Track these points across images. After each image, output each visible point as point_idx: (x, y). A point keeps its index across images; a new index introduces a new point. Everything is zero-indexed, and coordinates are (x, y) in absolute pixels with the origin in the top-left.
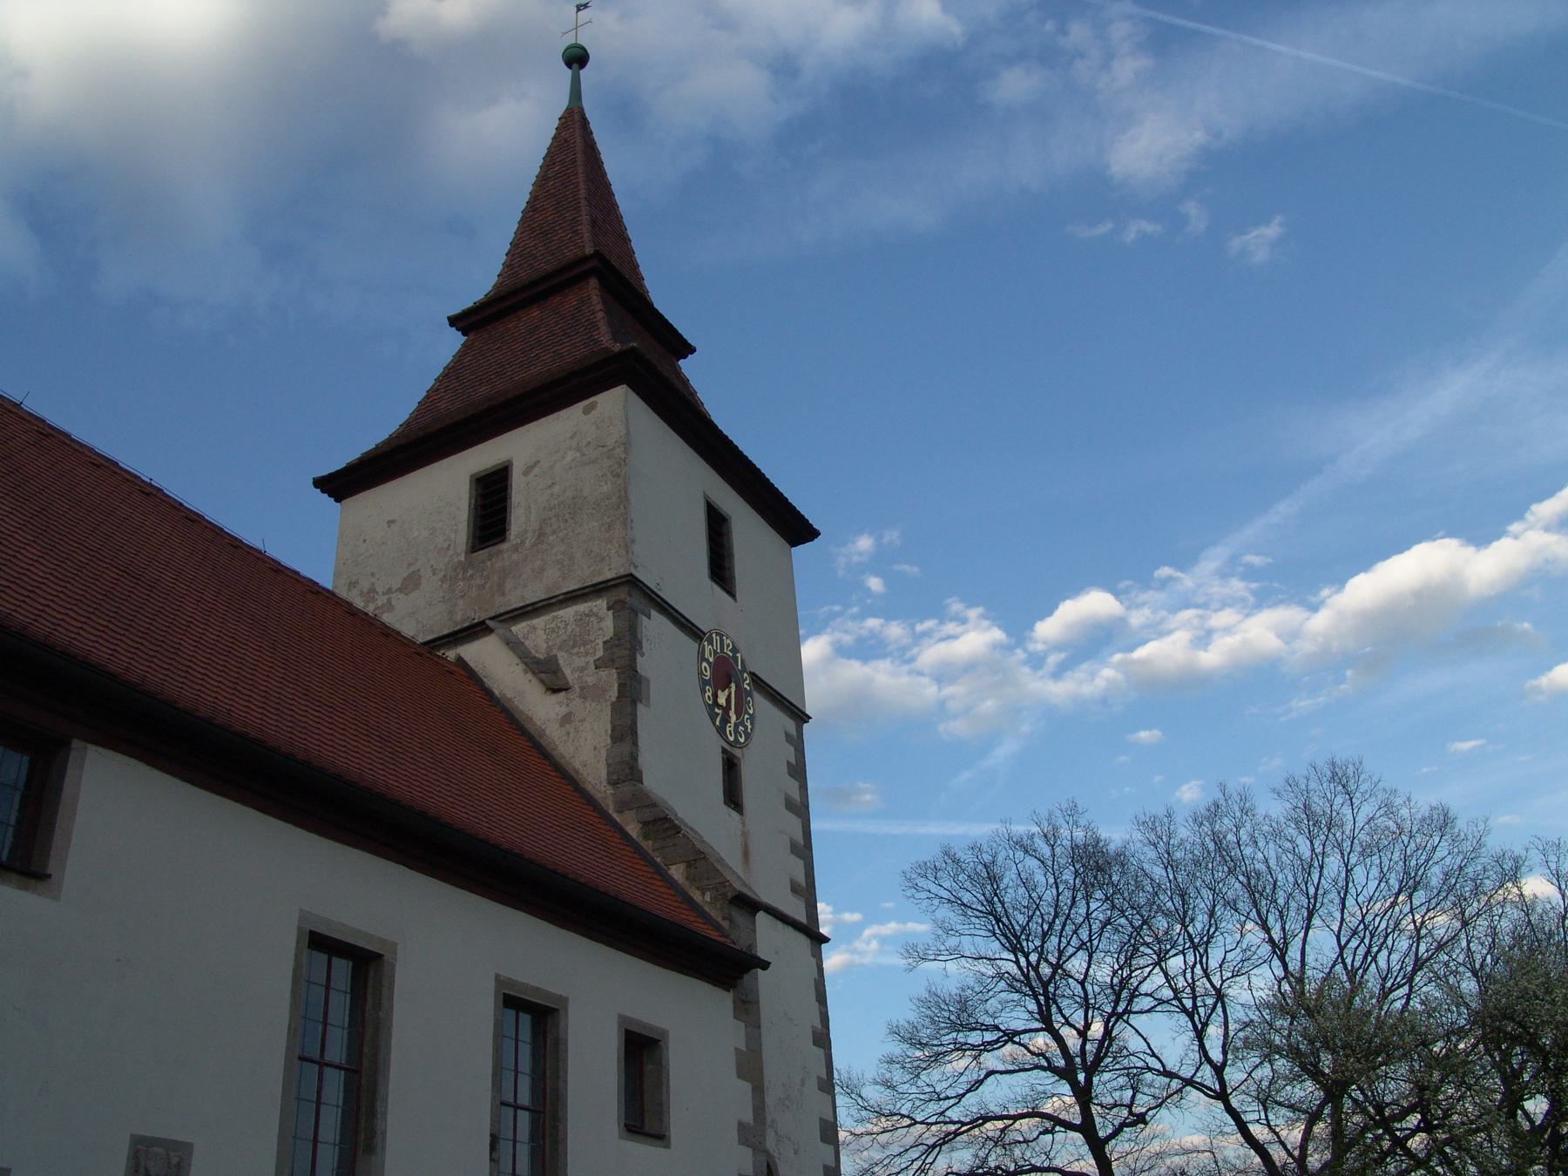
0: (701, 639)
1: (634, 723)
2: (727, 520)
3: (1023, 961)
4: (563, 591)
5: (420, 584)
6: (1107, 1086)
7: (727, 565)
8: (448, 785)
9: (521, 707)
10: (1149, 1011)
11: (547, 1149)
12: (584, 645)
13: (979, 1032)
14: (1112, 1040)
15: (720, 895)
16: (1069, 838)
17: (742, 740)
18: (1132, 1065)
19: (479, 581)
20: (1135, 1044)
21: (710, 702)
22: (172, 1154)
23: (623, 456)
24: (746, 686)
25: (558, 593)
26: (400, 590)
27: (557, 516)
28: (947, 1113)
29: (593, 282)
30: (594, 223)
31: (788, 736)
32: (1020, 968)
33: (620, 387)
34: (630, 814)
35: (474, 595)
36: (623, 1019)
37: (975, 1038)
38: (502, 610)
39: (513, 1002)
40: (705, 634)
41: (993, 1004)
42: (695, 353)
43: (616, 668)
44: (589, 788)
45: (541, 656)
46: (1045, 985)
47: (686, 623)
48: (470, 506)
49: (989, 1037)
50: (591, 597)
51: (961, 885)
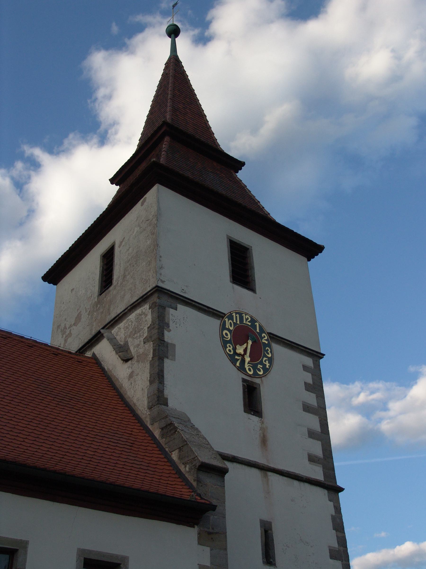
2: (248, 249)
12: (139, 332)
19: (101, 310)
23: (155, 222)
34: (156, 425)
36: (81, 552)
42: (245, 163)
44: (139, 413)
45: (122, 343)
47: (207, 309)
48: (100, 272)
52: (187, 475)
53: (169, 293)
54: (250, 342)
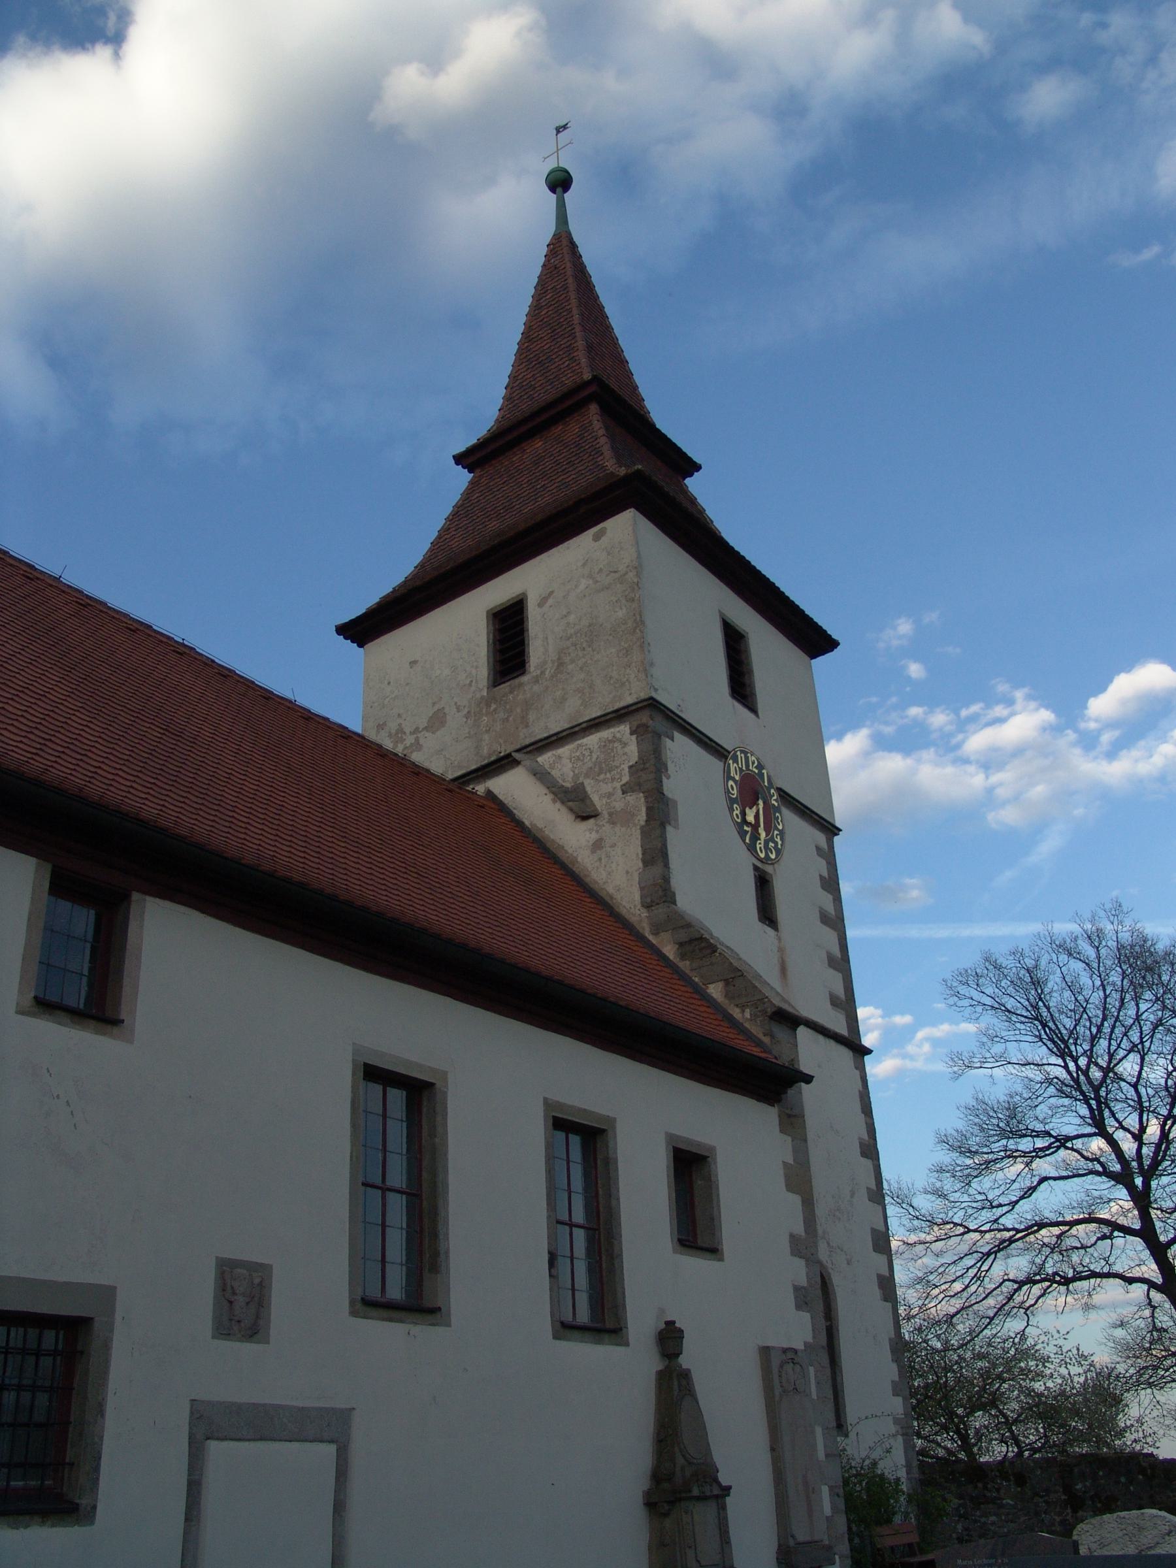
0: (726, 758)
1: (664, 846)
3: (1072, 1066)
4: (586, 719)
5: (446, 722)
9: (552, 837)
11: (604, 1266)
12: (610, 771)
15: (760, 1011)
17: (773, 856)
21: (739, 821)
23: (636, 580)
24: (774, 802)
25: (581, 721)
26: (426, 729)
28: (1001, 1221)
30: (590, 348)
31: (818, 849)
32: (1069, 1072)
36: (670, 1137)
37: (1025, 1144)
38: (528, 742)
40: (729, 753)
41: (1042, 1110)
43: (643, 793)
44: (624, 912)
45: (568, 785)
46: (1096, 1089)
47: (709, 742)
49: (1040, 1143)
51: (1003, 991)
52: (747, 1025)
53: (666, 710)
54: (761, 802)
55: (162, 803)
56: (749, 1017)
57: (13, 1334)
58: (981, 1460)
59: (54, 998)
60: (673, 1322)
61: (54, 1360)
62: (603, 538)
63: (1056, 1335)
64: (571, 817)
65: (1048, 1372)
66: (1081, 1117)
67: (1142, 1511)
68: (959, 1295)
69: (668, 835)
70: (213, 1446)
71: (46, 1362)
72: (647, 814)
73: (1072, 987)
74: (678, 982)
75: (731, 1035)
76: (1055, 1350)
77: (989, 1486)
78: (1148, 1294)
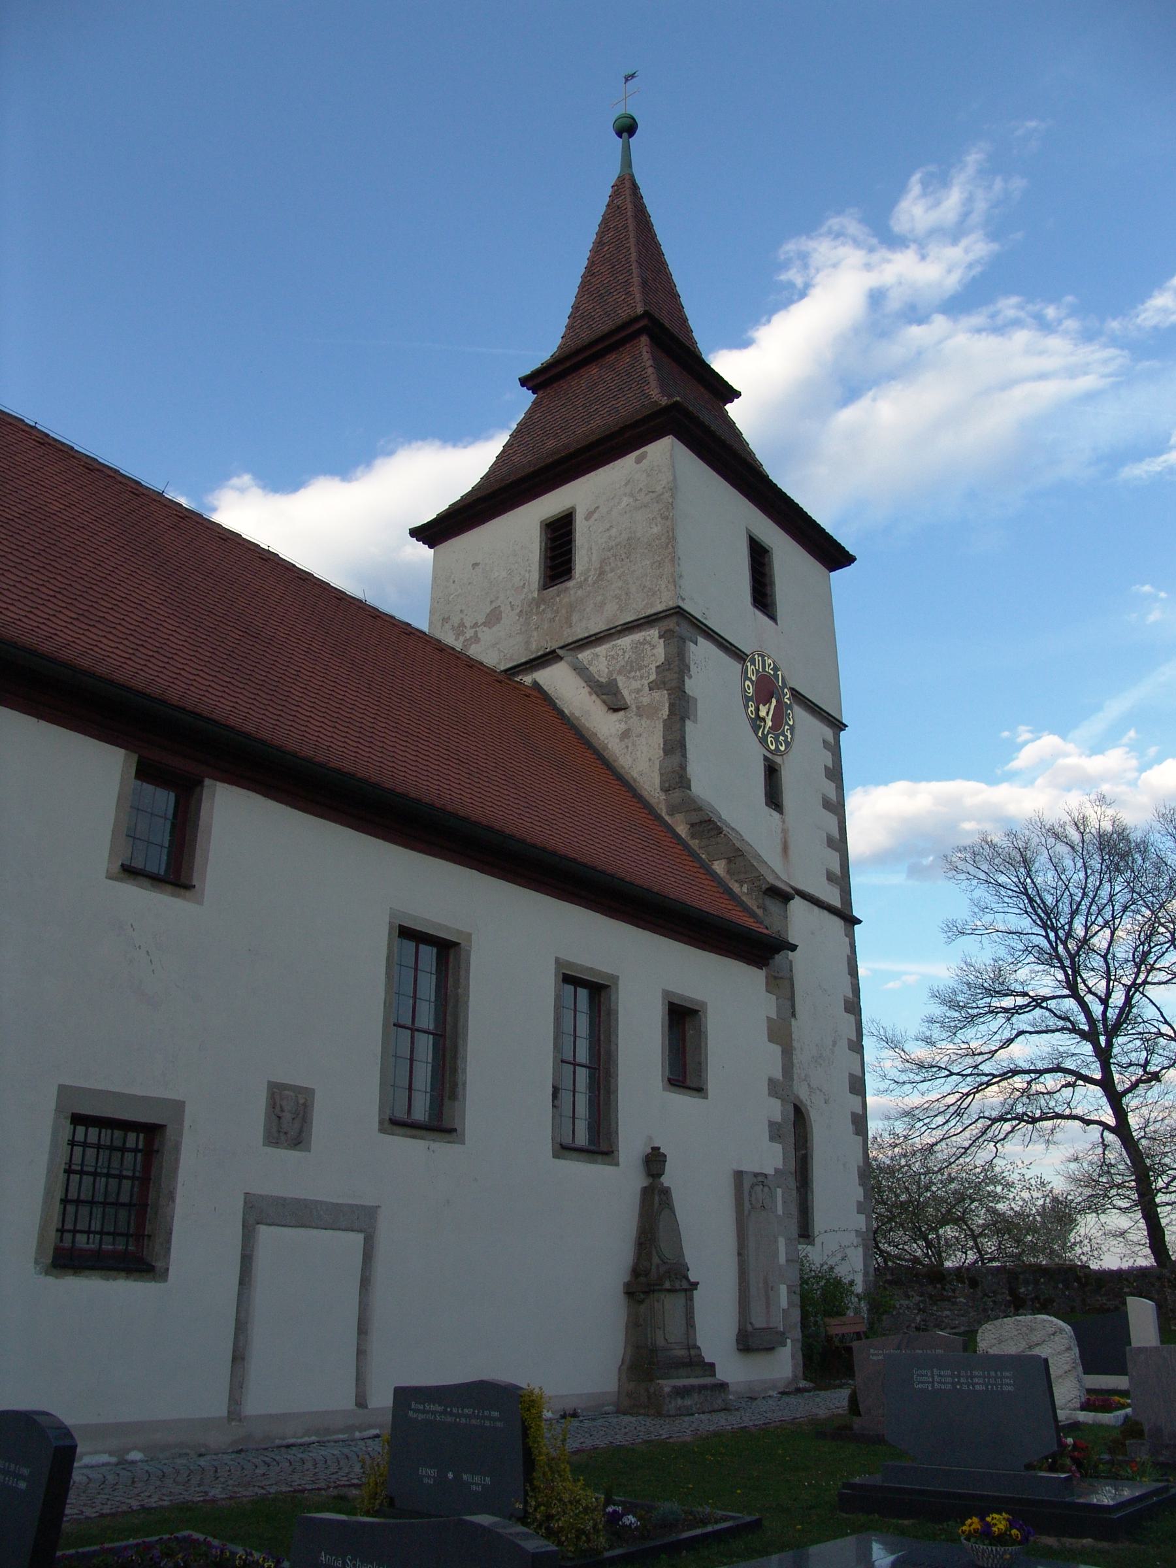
0: (744, 660)
1: (684, 738)
3: (1052, 935)
4: (621, 623)
6: (1125, 1047)
7: (769, 592)
8: (517, 799)
9: (587, 725)
10: (1166, 983)
11: (602, 1098)
12: (639, 670)
13: (1013, 997)
14: (1131, 1007)
16: (1098, 827)
17: (782, 748)
18: (1147, 1031)
20: (1150, 1013)
21: (753, 716)
22: (300, 1096)
23: (670, 501)
24: (786, 700)
26: (484, 624)
27: (615, 556)
28: (980, 1067)
29: (644, 339)
30: (644, 284)
32: (1050, 942)
33: (667, 437)
34: (679, 817)
35: (545, 628)
36: (666, 993)
37: (1008, 1002)
38: (570, 640)
39: (570, 979)
43: (667, 690)
44: (645, 794)
45: (603, 680)
46: (1072, 957)
48: (540, 549)
49: (1021, 1001)
50: (645, 627)
51: (996, 868)
52: (744, 898)
54: (774, 701)
55: (235, 700)
56: (746, 891)
57: (103, 1135)
58: (948, 1264)
59: (138, 864)
60: (659, 1148)
61: (135, 1156)
62: (644, 461)
63: (1020, 1165)
64: (605, 708)
65: (1011, 1196)
66: (1059, 981)
67: (1036, 1316)
68: (940, 1128)
69: (687, 729)
70: (262, 1229)
71: (129, 1157)
72: (670, 710)
73: (1058, 869)
74: (687, 858)
75: (730, 907)
76: (1018, 1177)
77: (947, 1287)
78: (1102, 1134)
